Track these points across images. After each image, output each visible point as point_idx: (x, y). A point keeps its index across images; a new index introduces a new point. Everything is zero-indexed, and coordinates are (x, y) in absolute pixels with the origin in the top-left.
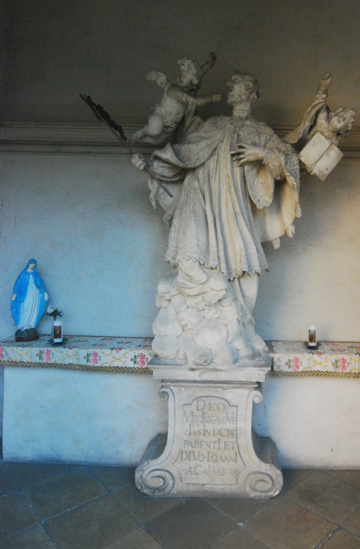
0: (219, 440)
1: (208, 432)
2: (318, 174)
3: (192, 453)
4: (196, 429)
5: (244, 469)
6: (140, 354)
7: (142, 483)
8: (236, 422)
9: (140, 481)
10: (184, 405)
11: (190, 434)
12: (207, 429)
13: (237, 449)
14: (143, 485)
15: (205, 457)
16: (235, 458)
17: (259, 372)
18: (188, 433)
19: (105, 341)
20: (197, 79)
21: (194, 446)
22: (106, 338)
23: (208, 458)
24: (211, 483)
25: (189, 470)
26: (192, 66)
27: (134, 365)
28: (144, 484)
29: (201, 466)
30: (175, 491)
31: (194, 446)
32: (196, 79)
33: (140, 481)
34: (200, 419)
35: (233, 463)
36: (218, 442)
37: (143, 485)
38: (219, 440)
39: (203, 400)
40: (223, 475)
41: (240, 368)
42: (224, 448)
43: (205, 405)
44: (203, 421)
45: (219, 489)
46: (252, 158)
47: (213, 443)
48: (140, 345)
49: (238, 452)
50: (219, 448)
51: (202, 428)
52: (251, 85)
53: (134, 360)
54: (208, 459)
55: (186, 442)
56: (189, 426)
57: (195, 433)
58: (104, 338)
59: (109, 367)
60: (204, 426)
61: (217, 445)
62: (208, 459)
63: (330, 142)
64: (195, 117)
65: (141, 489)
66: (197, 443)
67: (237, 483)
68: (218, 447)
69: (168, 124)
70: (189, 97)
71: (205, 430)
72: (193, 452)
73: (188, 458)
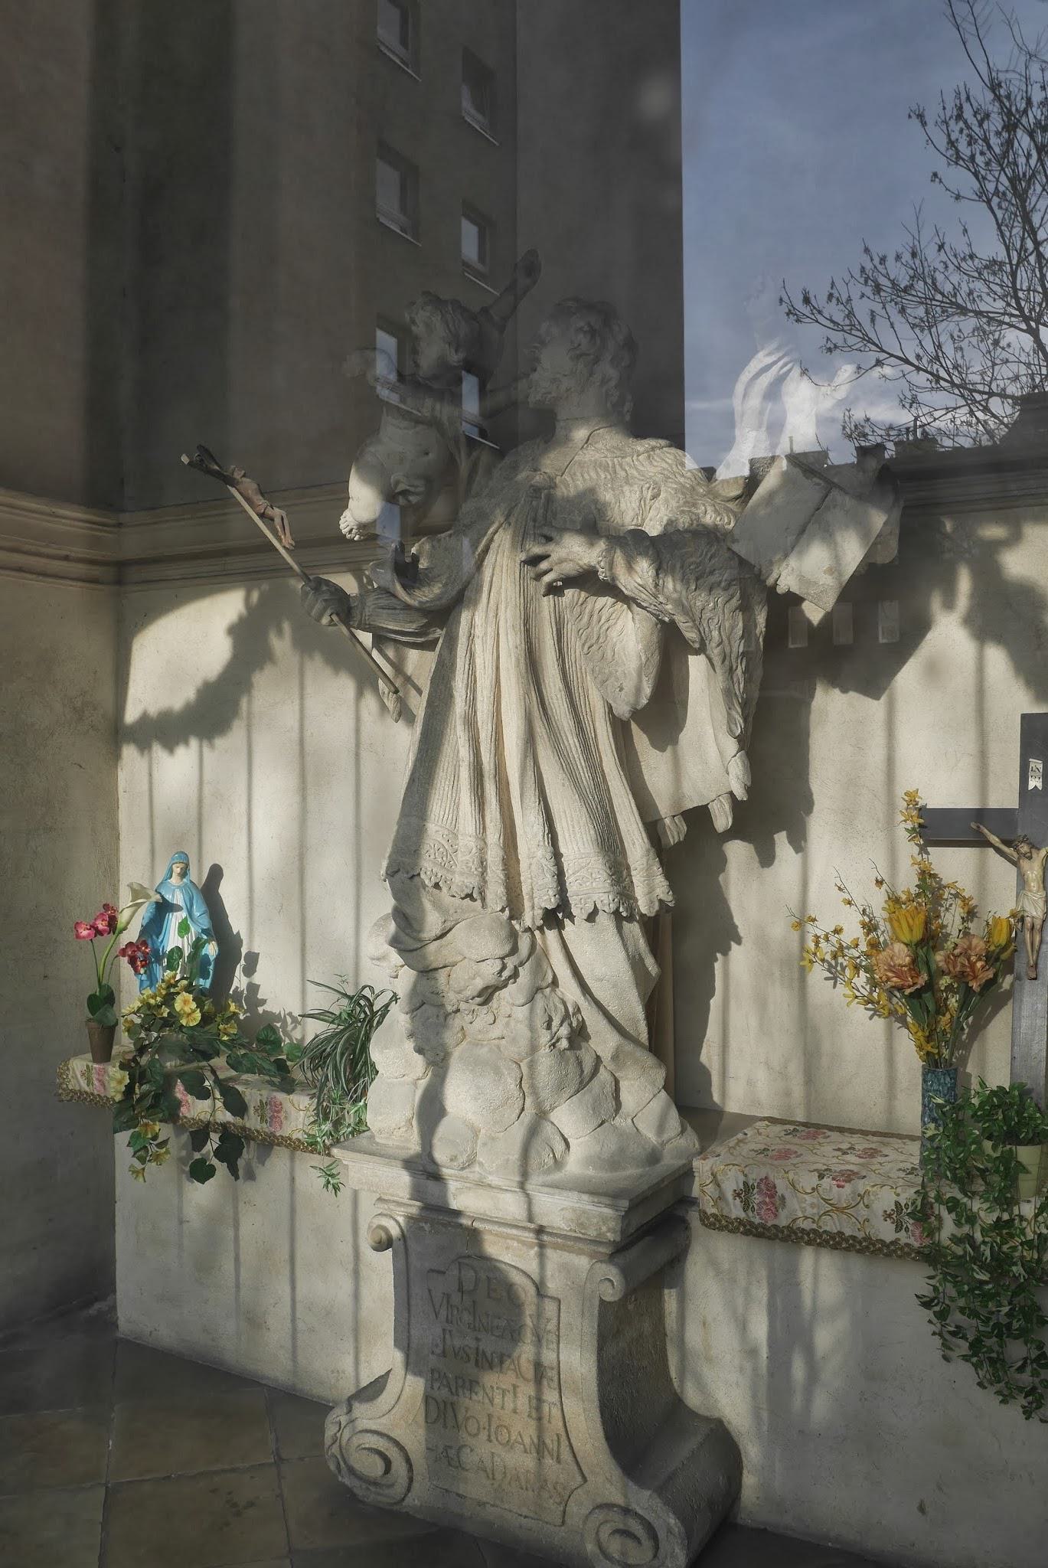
0: (515, 1387)
1: (487, 1360)
2: (800, 588)
3: (449, 1406)
4: (458, 1343)
5: (581, 1486)
6: (761, 1180)
7: (339, 1457)
8: (555, 1346)
9: (335, 1449)
10: (432, 1271)
11: (444, 1354)
12: (483, 1351)
13: (561, 1424)
14: (342, 1463)
15: (482, 1427)
16: (555, 1448)
17: (600, 1209)
18: (438, 1351)
19: (796, 1140)
20: (456, 351)
21: (454, 1390)
22: (800, 1128)
23: (489, 1430)
24: (498, 1502)
25: (444, 1454)
26: (437, 320)
27: (898, 1235)
28: (345, 1463)
29: (472, 1450)
30: (416, 1501)
31: (454, 1390)
32: (453, 351)
33: (335, 1449)
34: (467, 1317)
35: (551, 1461)
36: (511, 1392)
37: (342, 1463)
38: (515, 1387)
39: (473, 1268)
40: (527, 1489)
41: (546, 1189)
42: (527, 1414)
43: (477, 1281)
44: (475, 1326)
45: (521, 1527)
46: (569, 569)
47: (501, 1392)
48: (765, 1149)
49: (563, 1434)
50: (515, 1411)
51: (473, 1344)
52: (583, 339)
53: (894, 1216)
54: (489, 1436)
55: (436, 1375)
56: (439, 1331)
57: (456, 1355)
58: (792, 1128)
59: (814, 1231)
60: (478, 1339)
61: (509, 1398)
62: (489, 1436)
63: (819, 484)
64: (475, 454)
65: (337, 1472)
66: (460, 1382)
67: (563, 1523)
68: (512, 1405)
69: (401, 487)
70: (438, 406)
71: (481, 1352)
72: (452, 1404)
73: (442, 1420)
